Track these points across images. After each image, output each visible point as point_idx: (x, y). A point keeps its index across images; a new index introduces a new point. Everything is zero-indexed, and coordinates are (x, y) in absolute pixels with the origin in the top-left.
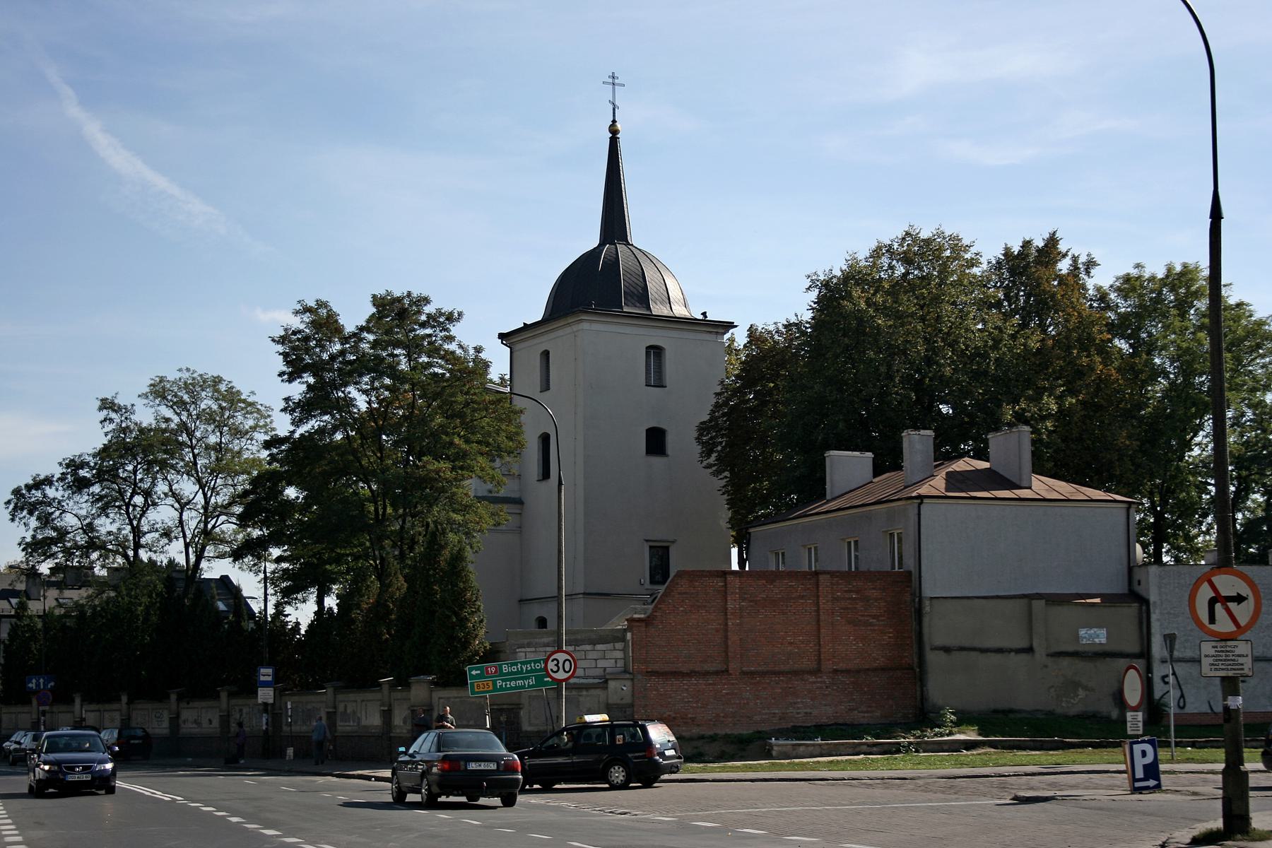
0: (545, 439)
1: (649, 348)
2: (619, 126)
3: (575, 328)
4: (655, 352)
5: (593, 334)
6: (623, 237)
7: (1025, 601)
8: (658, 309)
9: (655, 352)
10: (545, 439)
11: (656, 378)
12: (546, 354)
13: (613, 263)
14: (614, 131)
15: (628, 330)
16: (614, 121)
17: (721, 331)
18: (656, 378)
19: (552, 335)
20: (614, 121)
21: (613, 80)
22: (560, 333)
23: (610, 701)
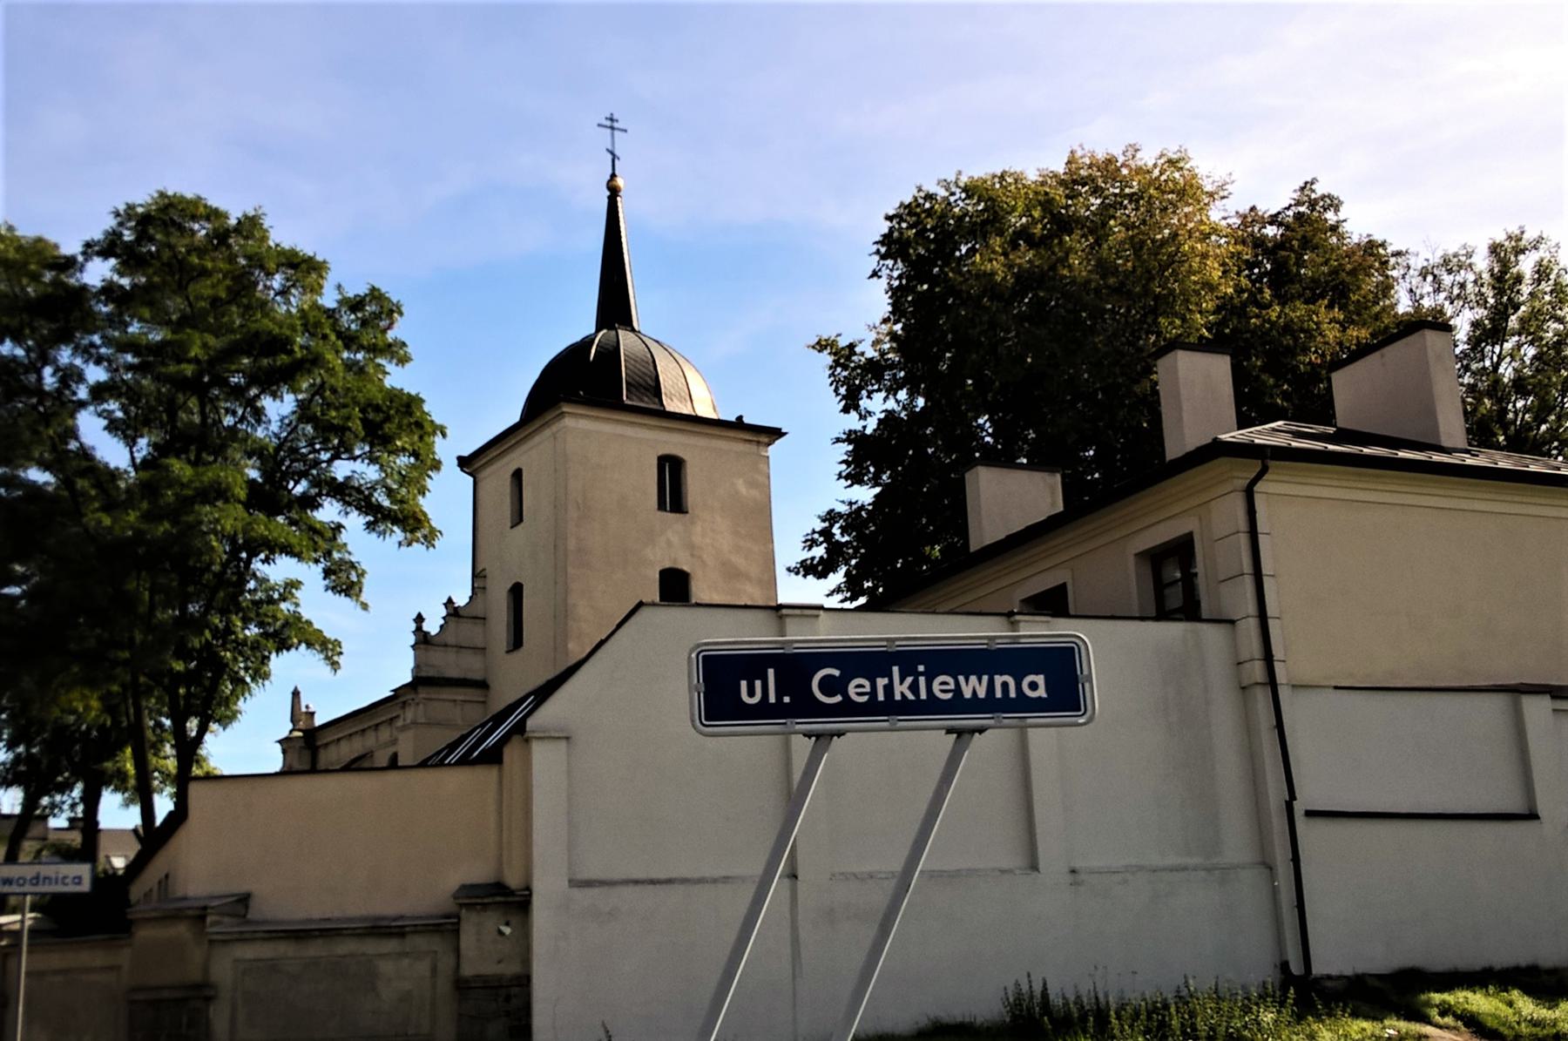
0: (516, 591)
1: (663, 460)
2: (620, 182)
3: (554, 428)
4: (671, 470)
5: (580, 427)
6: (627, 322)
7: (1499, 702)
8: (671, 406)
9: (671, 470)
10: (516, 591)
11: (672, 495)
12: (518, 475)
13: (610, 354)
14: (614, 192)
15: (629, 431)
16: (613, 176)
17: (765, 439)
18: (672, 495)
19: (525, 447)
20: (613, 176)
21: (611, 124)
22: (537, 439)
23: (467, 971)
